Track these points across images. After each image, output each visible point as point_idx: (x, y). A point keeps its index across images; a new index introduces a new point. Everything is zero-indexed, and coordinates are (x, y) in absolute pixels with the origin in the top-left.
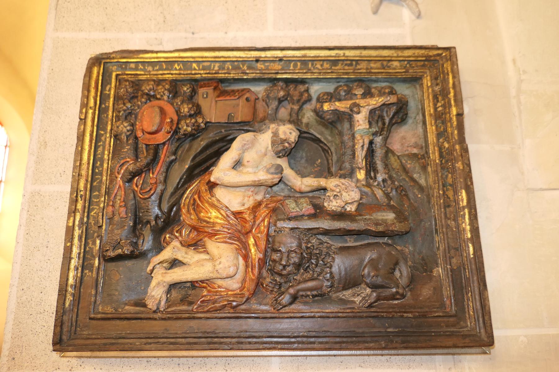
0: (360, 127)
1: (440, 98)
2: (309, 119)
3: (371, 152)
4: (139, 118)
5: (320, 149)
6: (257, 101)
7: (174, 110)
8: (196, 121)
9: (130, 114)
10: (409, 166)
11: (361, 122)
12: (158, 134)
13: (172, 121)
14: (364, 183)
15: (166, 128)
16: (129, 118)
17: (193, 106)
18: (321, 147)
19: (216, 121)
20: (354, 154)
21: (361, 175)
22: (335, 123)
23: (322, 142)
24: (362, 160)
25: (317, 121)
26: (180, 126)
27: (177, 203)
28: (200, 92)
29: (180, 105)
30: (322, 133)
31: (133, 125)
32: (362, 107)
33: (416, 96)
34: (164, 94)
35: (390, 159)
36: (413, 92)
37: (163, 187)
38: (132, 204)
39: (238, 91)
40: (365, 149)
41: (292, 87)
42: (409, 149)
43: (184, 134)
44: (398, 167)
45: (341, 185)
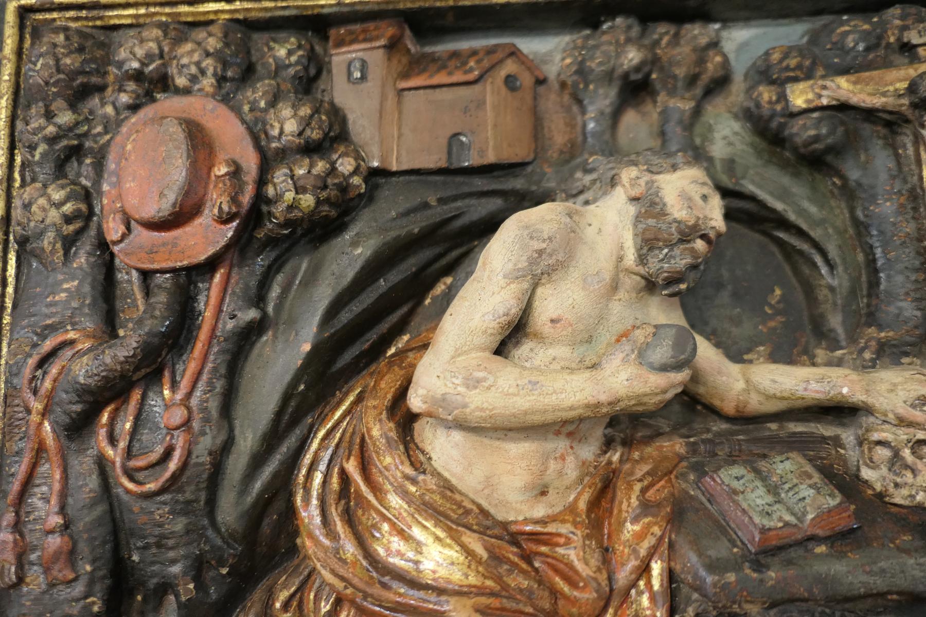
2: (730, 144)
4: (113, 166)
5: (774, 249)
6: (541, 89)
7: (241, 129)
8: (333, 170)
9: (76, 152)
12: (188, 229)
13: (236, 172)
15: (218, 200)
16: (72, 167)
17: (317, 111)
18: (780, 243)
19: (405, 167)
23: (783, 223)
26: (270, 191)
27: (281, 490)
28: (335, 59)
29: (265, 110)
30: (784, 195)
31: (87, 196)
34: (203, 72)
37: (220, 440)
38: (99, 522)
39: (474, 53)
43: (288, 223)
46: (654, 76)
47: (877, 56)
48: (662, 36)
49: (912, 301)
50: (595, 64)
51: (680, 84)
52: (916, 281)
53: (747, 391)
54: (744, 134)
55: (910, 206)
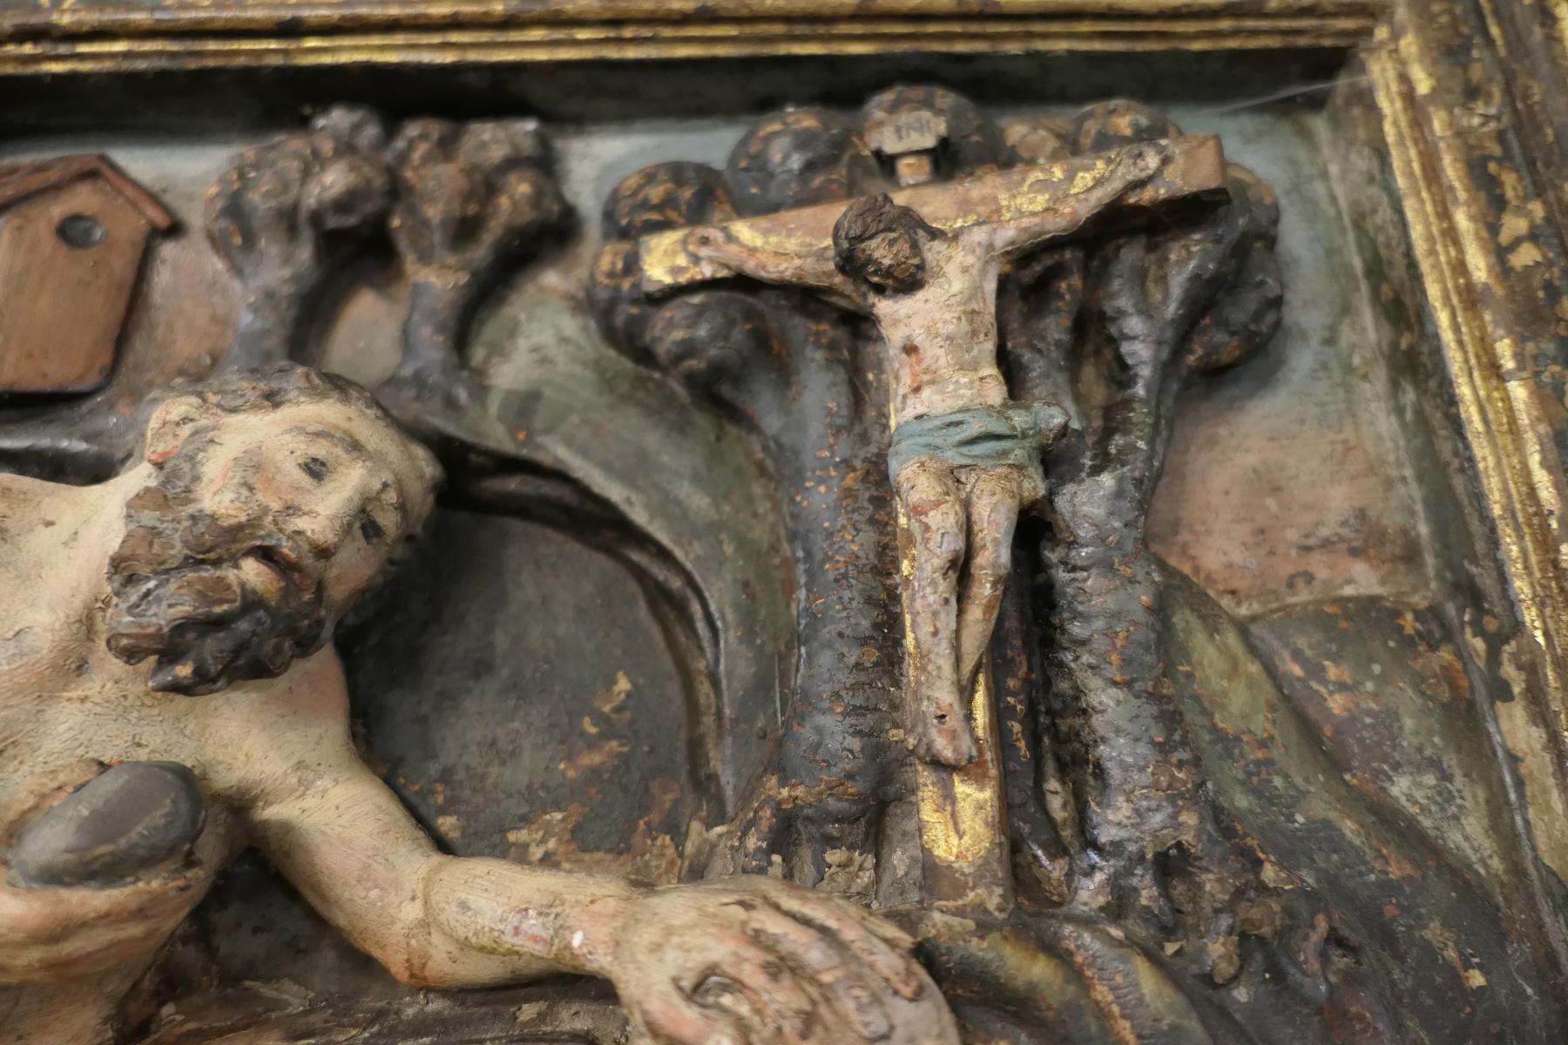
0: (931, 401)
1: (1510, 183)
2: (545, 361)
3: (1032, 609)
5: (633, 587)
10: (1337, 704)
11: (936, 354)
14: (993, 898)
18: (640, 574)
20: (888, 630)
21: (956, 825)
22: (737, 380)
23: (643, 540)
24: (966, 693)
25: (607, 382)
30: (636, 470)
32: (935, 234)
33: (1319, 188)
35: (1186, 655)
36: (1292, 162)
40: (984, 589)
41: (418, 133)
42: (1319, 565)
44: (1261, 724)
45: (752, 975)
46: (396, 222)
47: (830, 181)
48: (411, 144)
49: (845, 714)
50: (259, 199)
51: (437, 238)
52: (858, 666)
53: (425, 924)
54: (583, 342)
55: (867, 495)
